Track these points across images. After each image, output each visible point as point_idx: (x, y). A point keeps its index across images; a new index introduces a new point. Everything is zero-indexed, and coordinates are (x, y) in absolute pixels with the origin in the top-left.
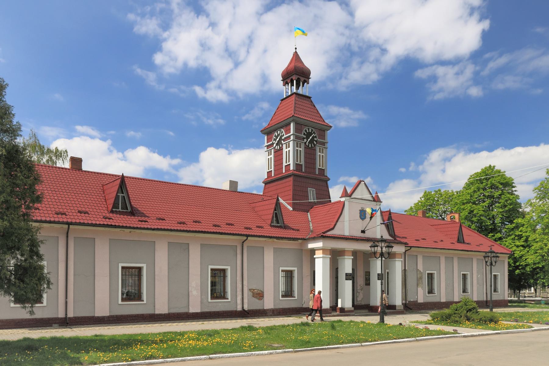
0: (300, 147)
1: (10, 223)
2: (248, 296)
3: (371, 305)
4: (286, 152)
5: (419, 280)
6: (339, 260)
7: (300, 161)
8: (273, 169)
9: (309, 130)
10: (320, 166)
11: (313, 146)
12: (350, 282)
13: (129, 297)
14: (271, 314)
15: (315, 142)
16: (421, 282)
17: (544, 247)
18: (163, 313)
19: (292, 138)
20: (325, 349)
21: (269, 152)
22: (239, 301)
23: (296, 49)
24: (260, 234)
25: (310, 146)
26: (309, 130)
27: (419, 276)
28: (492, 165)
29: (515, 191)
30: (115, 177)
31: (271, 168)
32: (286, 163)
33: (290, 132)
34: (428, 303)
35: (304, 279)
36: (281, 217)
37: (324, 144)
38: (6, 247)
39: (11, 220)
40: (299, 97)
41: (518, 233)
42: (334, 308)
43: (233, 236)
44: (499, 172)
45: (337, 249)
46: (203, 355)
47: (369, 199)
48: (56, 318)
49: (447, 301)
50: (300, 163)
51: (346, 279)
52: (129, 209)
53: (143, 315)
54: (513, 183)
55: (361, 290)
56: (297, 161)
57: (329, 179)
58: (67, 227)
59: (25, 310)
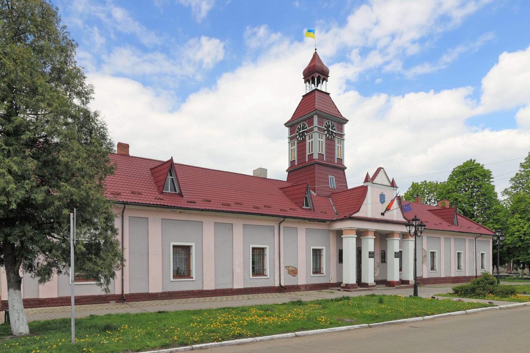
0: (322, 139)
1: (87, 193)
2: (284, 273)
3: (388, 280)
4: (309, 142)
5: (424, 257)
6: (362, 240)
7: (322, 152)
8: (296, 159)
9: (329, 123)
10: (338, 156)
11: (332, 138)
12: (398, 260)
13: (178, 274)
14: (304, 289)
15: (334, 134)
16: (425, 260)
17: (521, 229)
18: (211, 289)
19: (316, 129)
20: (393, 323)
21: (292, 143)
22: (277, 278)
23: (316, 49)
24: (295, 216)
25: (330, 138)
26: (329, 123)
27: (424, 255)
28: (473, 160)
29: (492, 182)
30: (159, 163)
31: (294, 158)
32: (309, 152)
33: (313, 125)
34: (431, 278)
35: (331, 257)
36: (311, 200)
37: (342, 135)
38: (81, 220)
39: (88, 190)
40: (322, 94)
41: (495, 217)
42: (360, 283)
43: (272, 217)
44: (479, 164)
45: (360, 230)
46: (288, 332)
47: (387, 185)
48: (113, 295)
49: (446, 276)
50: (322, 153)
51: (370, 257)
52: (178, 191)
53: (193, 291)
54: (491, 175)
55: (378, 267)
56: (319, 151)
57: (346, 168)
58: (123, 207)
59: (101, 287)
